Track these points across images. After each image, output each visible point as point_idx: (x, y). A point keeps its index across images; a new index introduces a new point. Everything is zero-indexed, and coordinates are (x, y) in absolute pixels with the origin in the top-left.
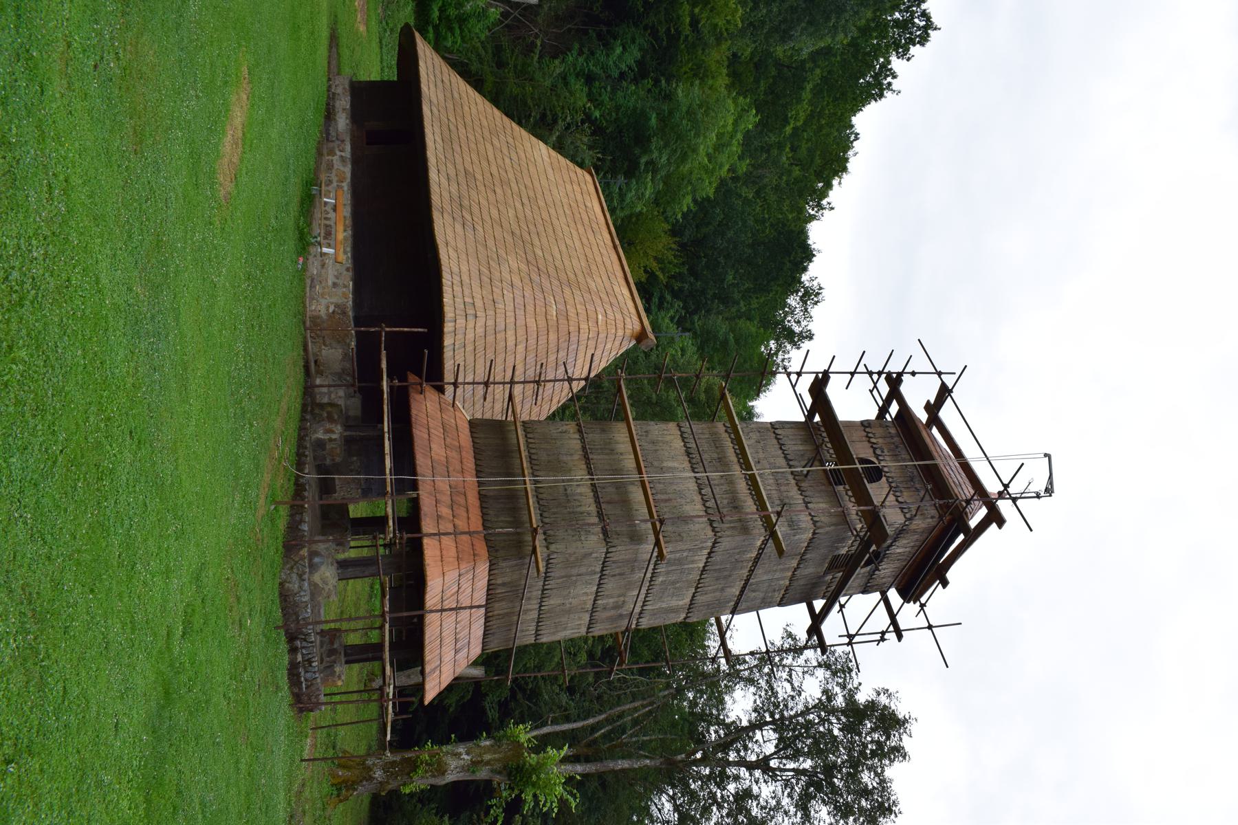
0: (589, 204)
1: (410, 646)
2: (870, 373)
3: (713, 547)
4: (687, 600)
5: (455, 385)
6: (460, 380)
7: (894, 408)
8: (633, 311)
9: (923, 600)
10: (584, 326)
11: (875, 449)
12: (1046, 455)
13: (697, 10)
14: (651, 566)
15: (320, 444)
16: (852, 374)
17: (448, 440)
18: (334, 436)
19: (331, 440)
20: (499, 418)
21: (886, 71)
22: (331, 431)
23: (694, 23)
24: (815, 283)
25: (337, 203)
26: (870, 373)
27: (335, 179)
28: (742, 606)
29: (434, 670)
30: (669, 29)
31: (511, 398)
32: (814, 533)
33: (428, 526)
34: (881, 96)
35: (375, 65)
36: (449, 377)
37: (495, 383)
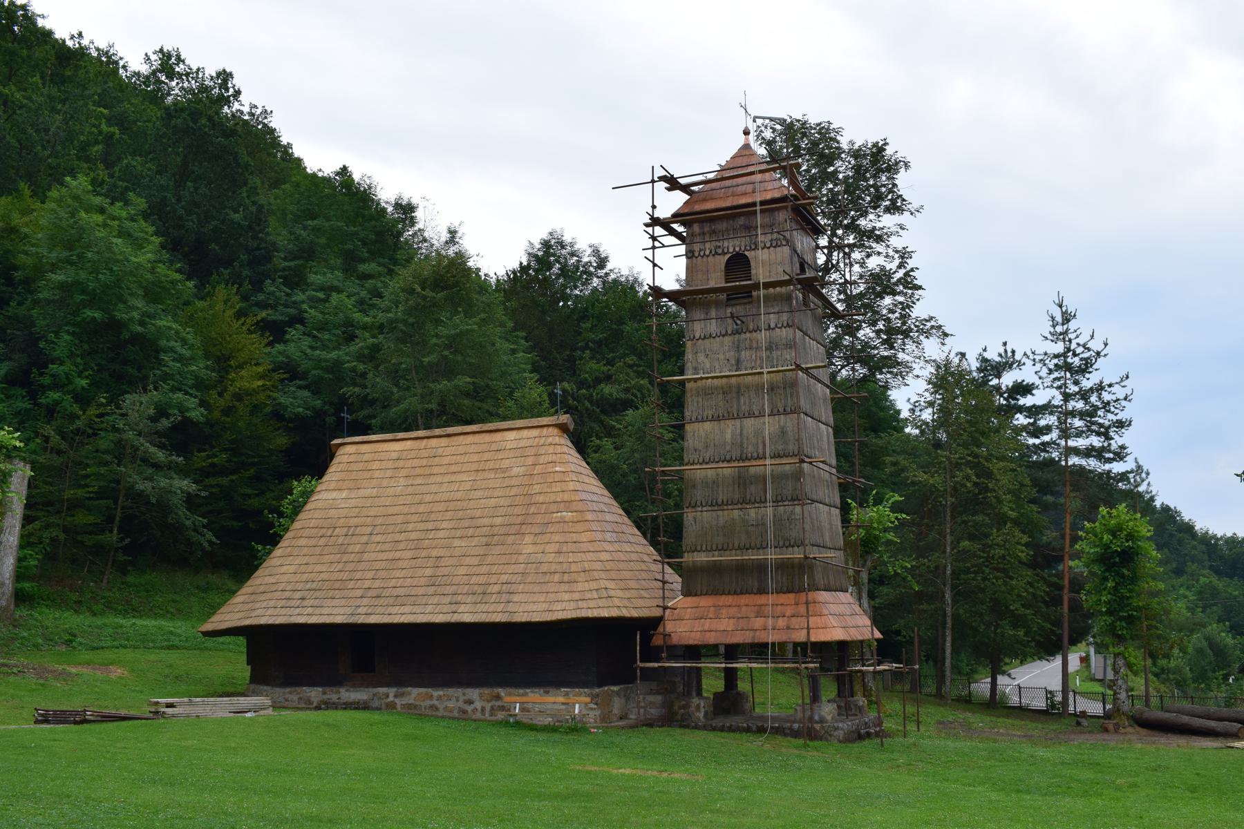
0: (395, 455)
2: (654, 248)
8: (535, 432)
10: (571, 486)
11: (716, 253)
16: (655, 265)
17: (711, 615)
22: (698, 706)
24: (154, 57)
25: (520, 701)
26: (654, 248)
27: (429, 702)
33: (801, 637)
34: (273, 131)
35: (234, 662)
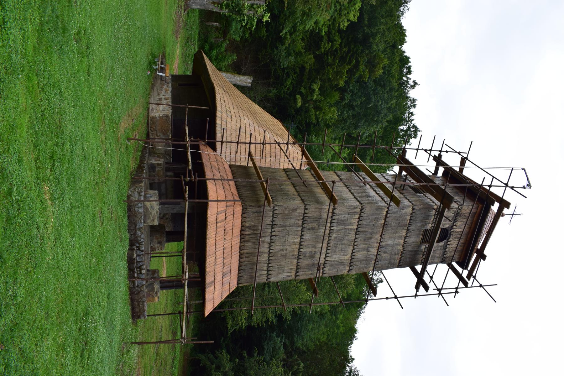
1: (199, 285)
3: (361, 212)
4: (349, 256)
5: (222, 142)
6: (224, 140)
7: (441, 170)
9: (474, 274)
12: (523, 169)
13: (317, 113)
14: (328, 225)
15: (152, 167)
18: (160, 162)
19: (159, 164)
20: (243, 164)
21: (406, 56)
23: (317, 119)
28: (380, 264)
29: (211, 282)
30: (306, 121)
31: (250, 154)
32: (413, 209)
36: (219, 136)
37: (241, 143)
